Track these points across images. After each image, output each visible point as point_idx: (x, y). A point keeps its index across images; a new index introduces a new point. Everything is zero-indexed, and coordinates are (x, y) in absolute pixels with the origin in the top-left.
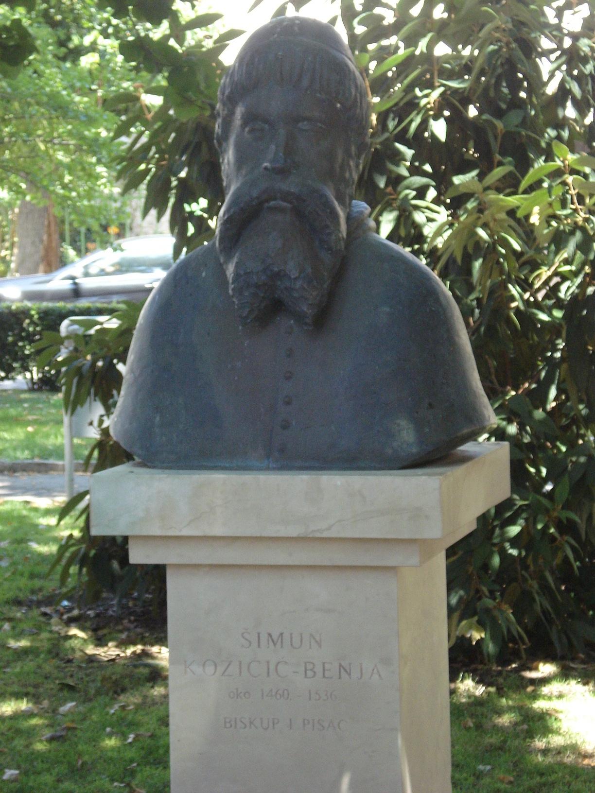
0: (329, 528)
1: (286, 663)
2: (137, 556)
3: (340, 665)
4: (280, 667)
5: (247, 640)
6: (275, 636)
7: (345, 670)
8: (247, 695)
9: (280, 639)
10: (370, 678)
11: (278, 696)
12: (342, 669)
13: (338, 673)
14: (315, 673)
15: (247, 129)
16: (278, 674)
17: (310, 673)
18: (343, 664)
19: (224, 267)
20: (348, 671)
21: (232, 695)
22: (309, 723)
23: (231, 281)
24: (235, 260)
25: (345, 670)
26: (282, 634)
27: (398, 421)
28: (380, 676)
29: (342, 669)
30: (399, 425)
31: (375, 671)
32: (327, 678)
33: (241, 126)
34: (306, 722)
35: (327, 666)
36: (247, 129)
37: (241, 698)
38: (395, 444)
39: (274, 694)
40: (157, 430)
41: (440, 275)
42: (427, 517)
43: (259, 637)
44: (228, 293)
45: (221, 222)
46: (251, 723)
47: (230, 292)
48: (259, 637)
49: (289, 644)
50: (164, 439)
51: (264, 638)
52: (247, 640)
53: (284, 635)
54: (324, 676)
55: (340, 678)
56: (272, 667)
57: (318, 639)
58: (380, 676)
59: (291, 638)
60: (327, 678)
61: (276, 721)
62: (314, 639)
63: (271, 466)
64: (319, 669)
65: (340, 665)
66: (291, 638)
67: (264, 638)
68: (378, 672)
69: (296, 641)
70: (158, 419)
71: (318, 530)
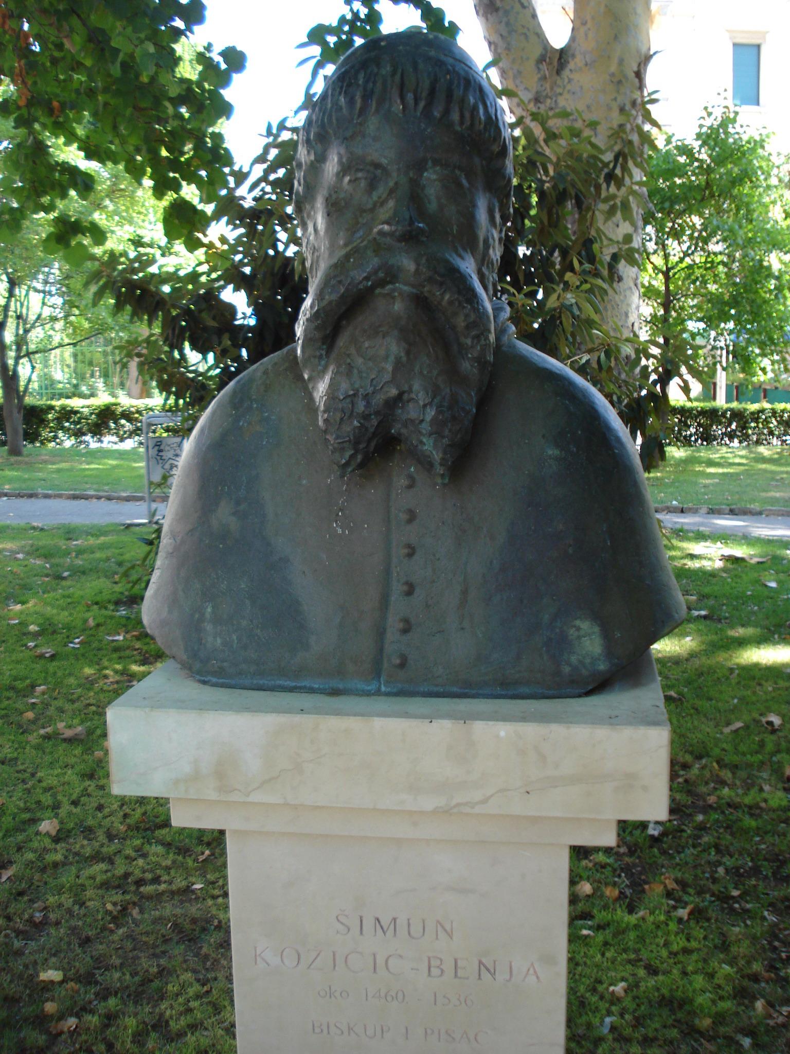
0: (485, 801)
1: (401, 956)
2: (180, 819)
3: (480, 963)
4: (391, 962)
5: (342, 923)
6: (385, 922)
7: (488, 970)
8: (344, 994)
9: (392, 926)
10: (524, 980)
11: (389, 998)
12: (482, 967)
13: (477, 971)
14: (442, 971)
15: (347, 179)
16: (387, 969)
17: (435, 972)
18: (484, 960)
19: (310, 386)
20: (492, 971)
21: (322, 993)
22: (433, 1031)
23: (322, 408)
24: (327, 378)
25: (488, 970)
26: (395, 919)
27: (578, 623)
28: (538, 977)
29: (482, 967)
30: (578, 629)
31: (531, 971)
32: (460, 978)
33: (338, 174)
34: (429, 1032)
35: (460, 963)
36: (347, 179)
37: (336, 997)
38: (574, 659)
39: (383, 994)
40: (209, 627)
41: (729, 387)
42: (645, 788)
43: (361, 921)
44: (317, 425)
45: (308, 315)
46: (350, 1029)
47: (321, 423)
48: (361, 921)
49: (406, 933)
50: (219, 641)
51: (369, 924)
52: (342, 923)
53: (398, 921)
54: (456, 976)
55: (480, 978)
56: (380, 961)
57: (448, 928)
58: (538, 977)
59: (409, 925)
60: (460, 978)
61: (385, 1029)
62: (443, 927)
63: (383, 689)
64: (448, 966)
65: (480, 963)
66: (409, 925)
67: (369, 924)
68: (535, 972)
69: (416, 929)
70: (209, 610)
71: (466, 804)
